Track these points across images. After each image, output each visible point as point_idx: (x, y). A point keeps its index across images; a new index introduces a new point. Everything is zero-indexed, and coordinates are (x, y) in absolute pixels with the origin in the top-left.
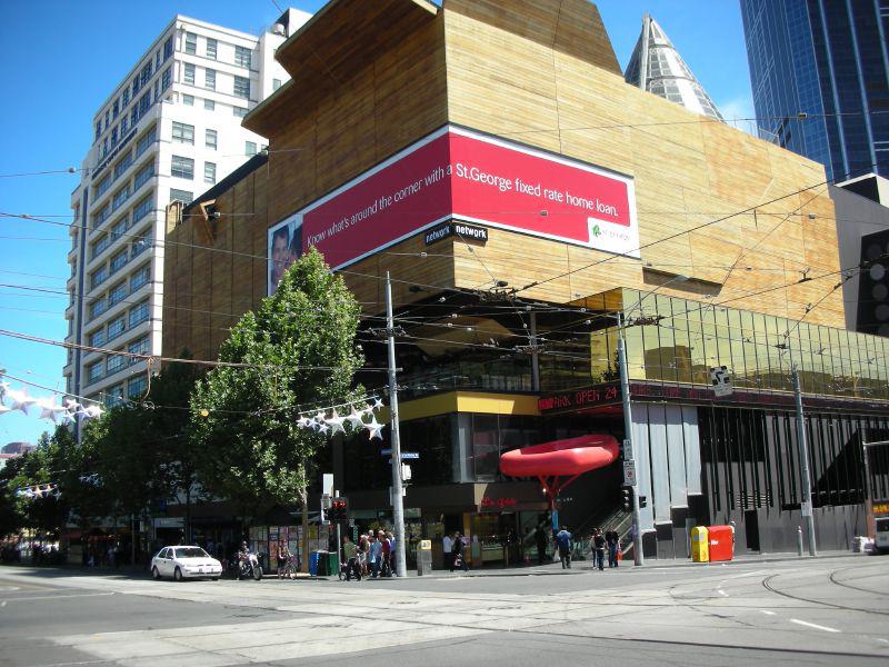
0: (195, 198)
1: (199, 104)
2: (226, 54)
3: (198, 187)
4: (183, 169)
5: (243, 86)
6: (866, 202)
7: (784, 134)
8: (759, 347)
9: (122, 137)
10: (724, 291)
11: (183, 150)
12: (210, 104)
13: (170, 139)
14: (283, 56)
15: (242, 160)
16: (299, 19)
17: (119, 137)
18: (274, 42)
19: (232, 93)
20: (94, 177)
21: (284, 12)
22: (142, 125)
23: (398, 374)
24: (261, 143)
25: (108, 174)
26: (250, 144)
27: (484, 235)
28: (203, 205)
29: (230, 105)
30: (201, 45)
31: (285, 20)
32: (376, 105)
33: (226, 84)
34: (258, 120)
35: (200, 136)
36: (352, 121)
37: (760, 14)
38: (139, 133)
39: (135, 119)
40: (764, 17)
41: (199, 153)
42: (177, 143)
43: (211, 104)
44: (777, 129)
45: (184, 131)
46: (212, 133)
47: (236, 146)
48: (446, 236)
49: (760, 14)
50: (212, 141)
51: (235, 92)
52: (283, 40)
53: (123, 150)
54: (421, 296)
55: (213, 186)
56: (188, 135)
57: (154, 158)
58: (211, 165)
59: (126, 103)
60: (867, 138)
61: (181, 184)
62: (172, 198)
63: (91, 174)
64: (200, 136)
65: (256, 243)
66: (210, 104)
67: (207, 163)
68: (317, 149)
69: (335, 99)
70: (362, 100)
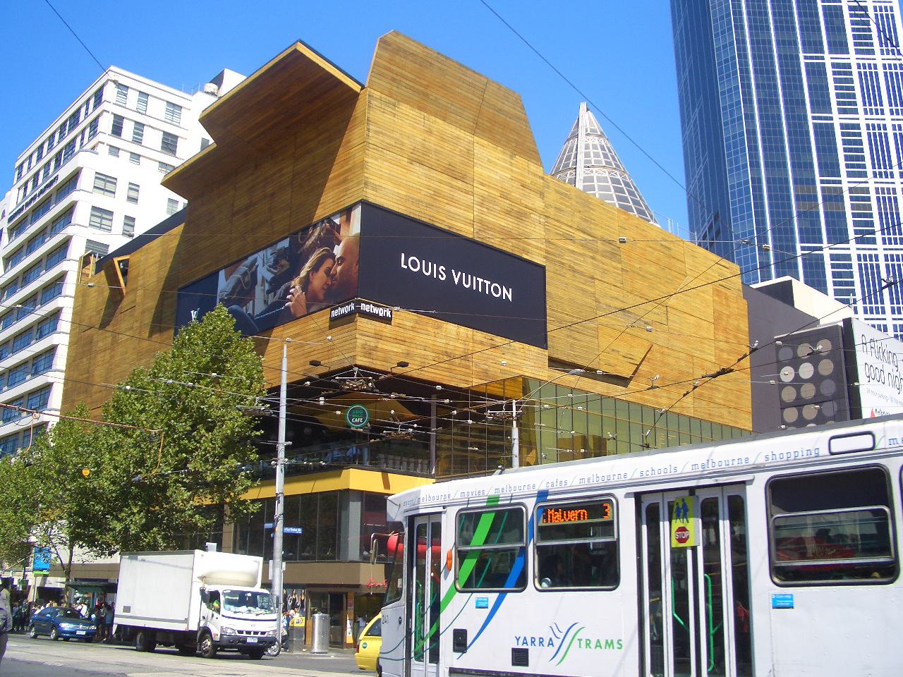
0: (110, 251)
1: (124, 156)
2: (156, 108)
3: (115, 241)
4: (101, 215)
5: (170, 143)
6: (779, 303)
7: (714, 231)
8: (625, 438)
9: (43, 182)
10: (632, 385)
11: (104, 201)
12: (136, 157)
13: (90, 188)
14: (209, 121)
15: (163, 216)
16: (233, 80)
17: (40, 182)
18: (202, 102)
19: (160, 150)
20: (10, 220)
21: (221, 71)
22: (64, 173)
23: (287, 448)
24: (182, 202)
25: (25, 217)
26: (204, 142)
27: (388, 314)
28: (116, 260)
29: (161, 131)
30: (133, 96)
31: (218, 80)
32: (294, 175)
33: (153, 139)
34: (177, 182)
35: (122, 190)
36: (269, 190)
37: (697, 110)
38: (59, 181)
39: (58, 166)
40: (700, 113)
41: (119, 205)
42: (98, 194)
43: (136, 157)
44: (707, 225)
45: (105, 183)
46: (134, 187)
47: (158, 205)
48: (351, 313)
49: (697, 110)
50: (133, 194)
51: (162, 148)
52: (214, 99)
53: (42, 196)
54: (321, 370)
55: (130, 240)
56: (109, 187)
57: (78, 173)
58: (130, 220)
59: (50, 148)
60: (793, 240)
61: (99, 236)
62: (87, 248)
63: (8, 216)
64: (122, 190)
65: (165, 303)
66: (136, 157)
67: (127, 217)
68: (234, 215)
69: (256, 166)
70: (281, 170)
